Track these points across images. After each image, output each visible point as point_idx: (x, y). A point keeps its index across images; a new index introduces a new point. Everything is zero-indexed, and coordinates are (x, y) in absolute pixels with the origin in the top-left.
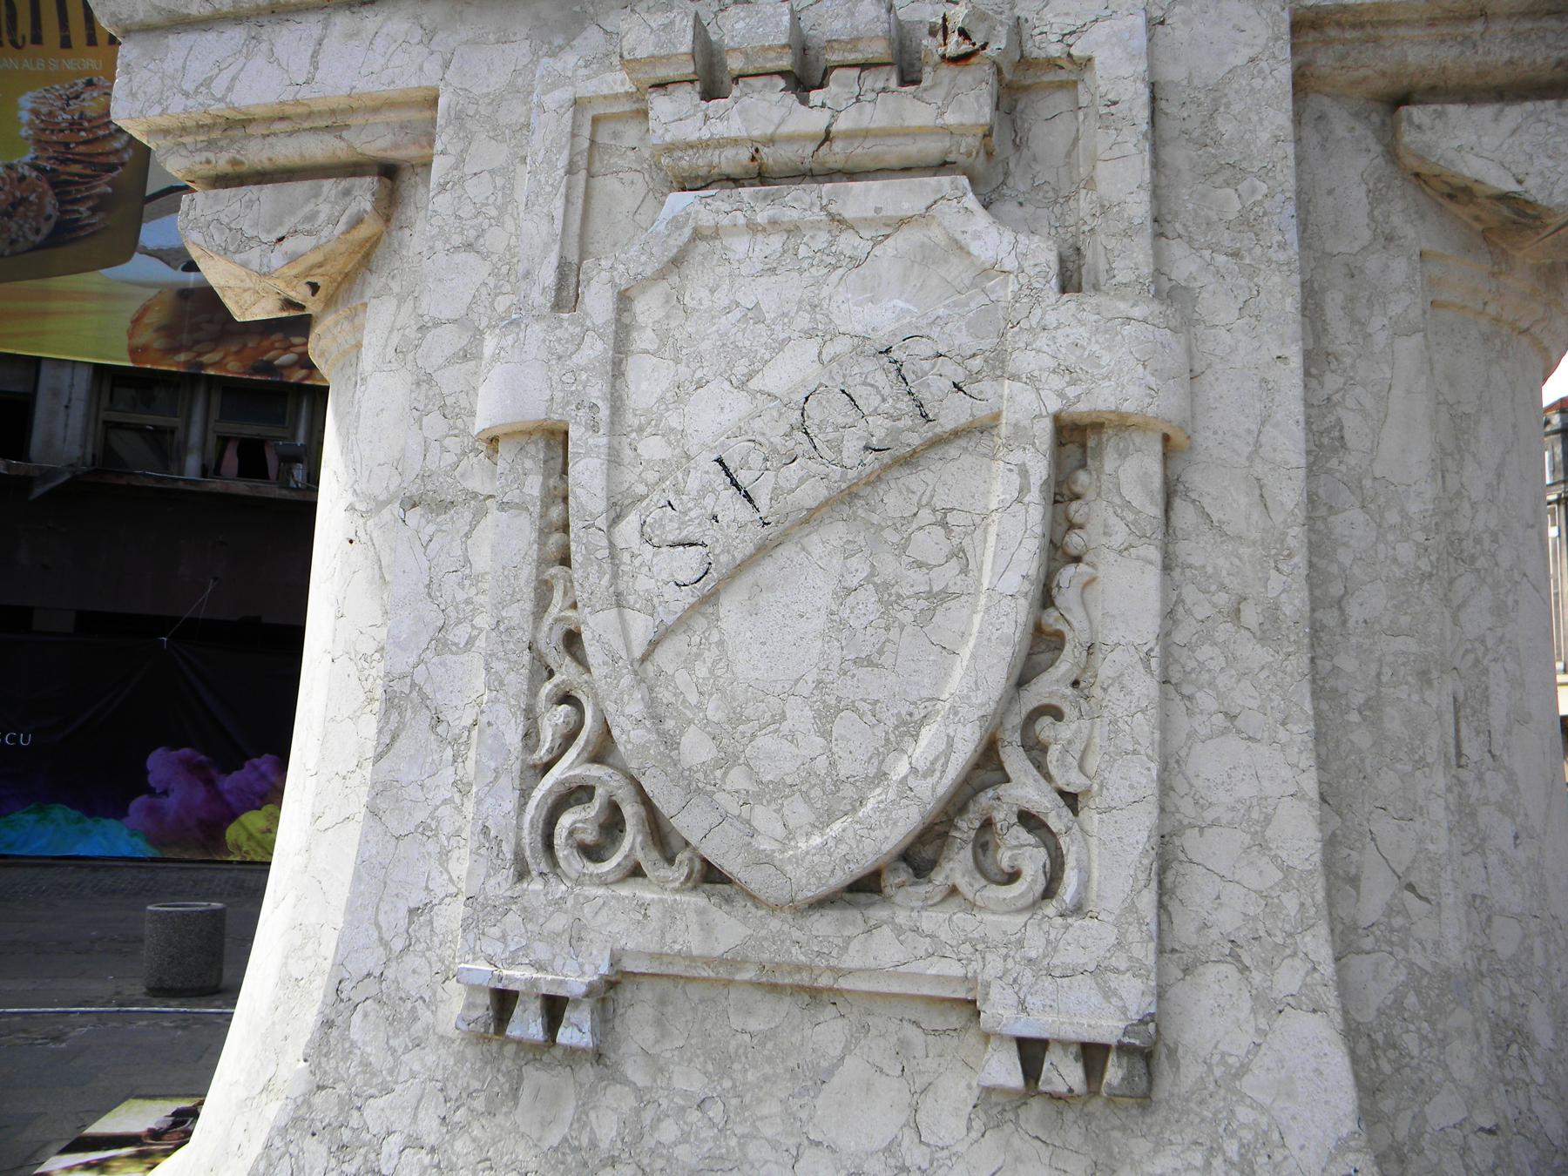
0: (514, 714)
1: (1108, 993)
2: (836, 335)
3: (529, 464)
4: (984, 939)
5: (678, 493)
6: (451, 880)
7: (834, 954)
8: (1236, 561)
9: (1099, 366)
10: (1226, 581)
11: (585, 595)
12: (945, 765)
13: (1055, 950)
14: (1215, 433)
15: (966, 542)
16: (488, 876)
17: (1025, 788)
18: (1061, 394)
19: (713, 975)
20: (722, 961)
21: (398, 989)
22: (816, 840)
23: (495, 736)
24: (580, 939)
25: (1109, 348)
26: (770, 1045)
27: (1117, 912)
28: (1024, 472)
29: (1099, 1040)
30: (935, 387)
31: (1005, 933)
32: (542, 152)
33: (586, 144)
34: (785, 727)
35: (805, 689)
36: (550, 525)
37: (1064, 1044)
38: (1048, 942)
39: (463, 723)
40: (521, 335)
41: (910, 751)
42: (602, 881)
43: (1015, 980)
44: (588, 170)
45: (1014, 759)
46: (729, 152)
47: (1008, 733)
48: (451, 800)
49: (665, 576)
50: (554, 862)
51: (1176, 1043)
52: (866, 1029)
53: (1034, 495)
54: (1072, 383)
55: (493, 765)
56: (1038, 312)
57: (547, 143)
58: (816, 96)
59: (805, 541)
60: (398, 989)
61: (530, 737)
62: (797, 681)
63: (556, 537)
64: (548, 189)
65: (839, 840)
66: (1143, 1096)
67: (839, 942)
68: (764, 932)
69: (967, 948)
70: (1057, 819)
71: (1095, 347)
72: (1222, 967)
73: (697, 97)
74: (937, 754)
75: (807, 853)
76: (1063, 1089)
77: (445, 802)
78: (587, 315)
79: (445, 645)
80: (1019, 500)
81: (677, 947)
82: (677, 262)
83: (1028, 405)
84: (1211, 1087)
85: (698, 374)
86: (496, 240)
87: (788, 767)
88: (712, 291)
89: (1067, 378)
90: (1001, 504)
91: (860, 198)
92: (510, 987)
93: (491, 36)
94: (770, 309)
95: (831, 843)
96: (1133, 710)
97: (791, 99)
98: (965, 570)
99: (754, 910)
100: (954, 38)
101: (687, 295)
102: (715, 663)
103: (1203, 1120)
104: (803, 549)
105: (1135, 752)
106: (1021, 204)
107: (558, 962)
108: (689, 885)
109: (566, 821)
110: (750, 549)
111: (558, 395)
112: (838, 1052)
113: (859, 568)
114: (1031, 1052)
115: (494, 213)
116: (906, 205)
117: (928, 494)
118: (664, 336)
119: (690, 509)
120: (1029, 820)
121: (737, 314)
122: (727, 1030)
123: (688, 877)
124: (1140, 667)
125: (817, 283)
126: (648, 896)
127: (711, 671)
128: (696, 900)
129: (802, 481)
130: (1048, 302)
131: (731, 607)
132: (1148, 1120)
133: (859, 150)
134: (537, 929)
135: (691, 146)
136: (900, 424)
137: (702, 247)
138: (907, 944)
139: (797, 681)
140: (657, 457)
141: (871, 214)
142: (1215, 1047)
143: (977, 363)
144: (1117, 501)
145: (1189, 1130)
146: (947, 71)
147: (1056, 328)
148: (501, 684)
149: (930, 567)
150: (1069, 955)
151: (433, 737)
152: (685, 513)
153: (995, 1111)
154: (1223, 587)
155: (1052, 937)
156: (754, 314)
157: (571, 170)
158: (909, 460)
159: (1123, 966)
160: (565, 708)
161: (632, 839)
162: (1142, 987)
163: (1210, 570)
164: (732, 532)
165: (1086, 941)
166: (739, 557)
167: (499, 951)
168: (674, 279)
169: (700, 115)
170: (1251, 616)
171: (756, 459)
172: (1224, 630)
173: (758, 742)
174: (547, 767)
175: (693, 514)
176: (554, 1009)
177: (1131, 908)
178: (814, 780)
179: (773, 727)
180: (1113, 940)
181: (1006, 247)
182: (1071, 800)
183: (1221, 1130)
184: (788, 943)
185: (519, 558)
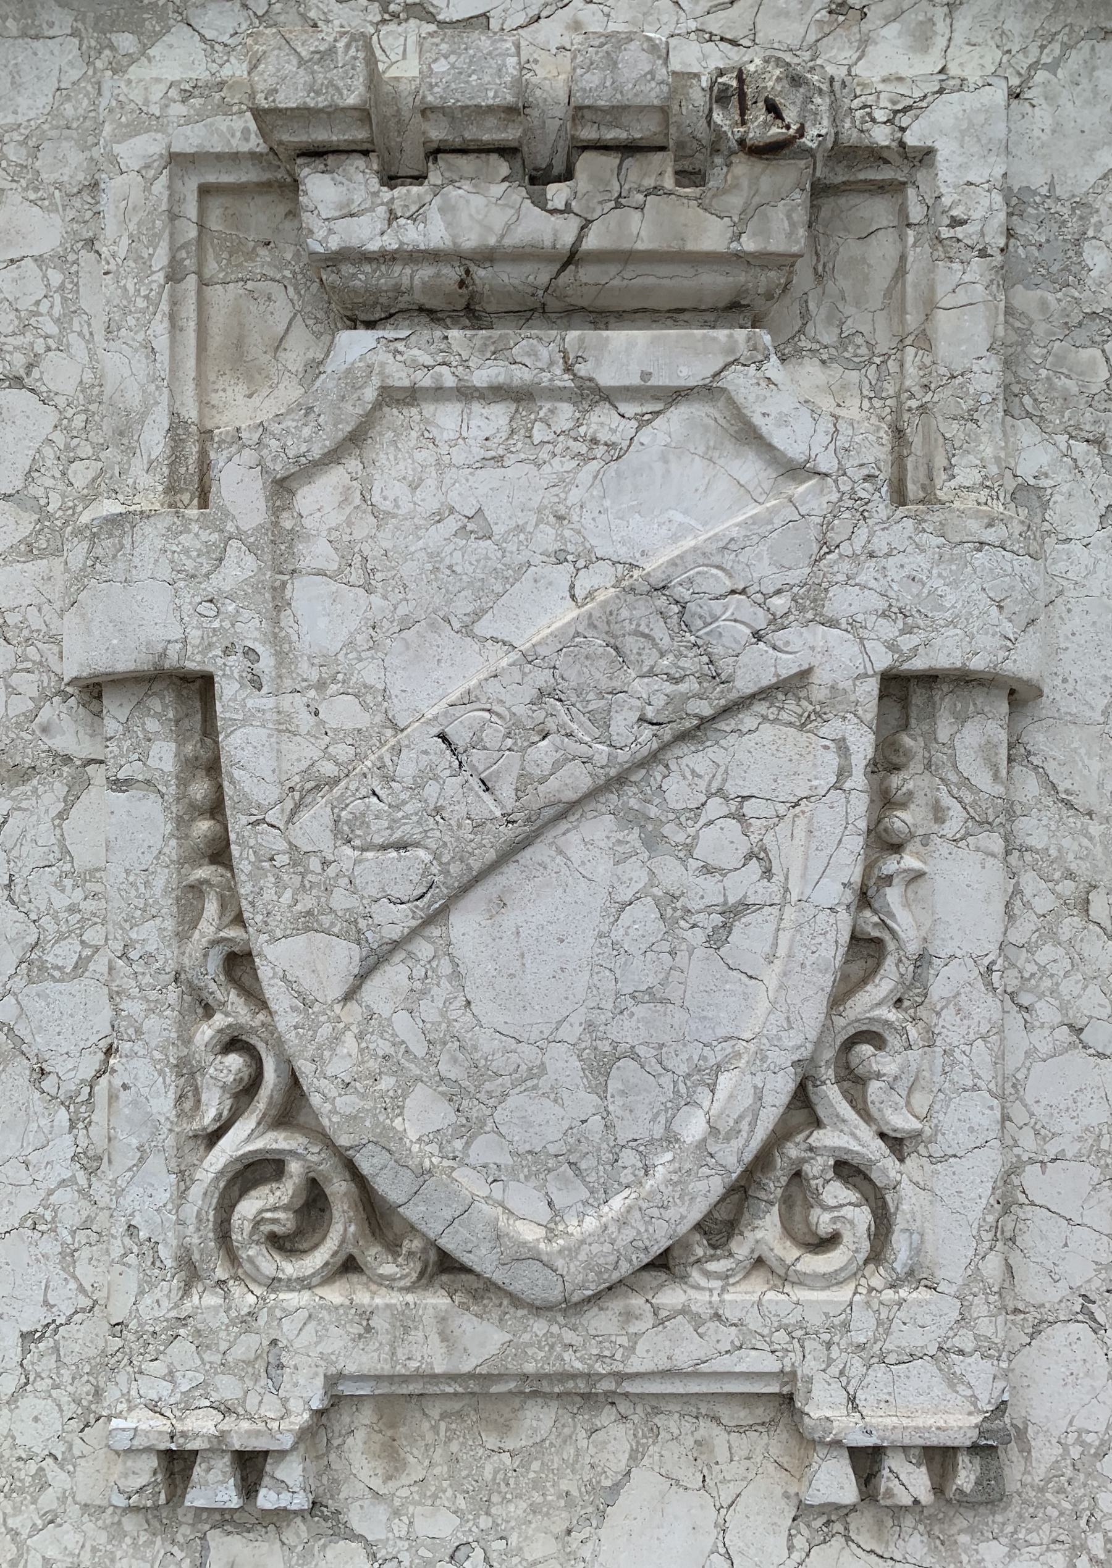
0: (161, 1073)
1: (953, 1380)
2: (592, 559)
3: (152, 725)
4: (801, 1324)
5: (388, 779)
6: (81, 1289)
7: (618, 1356)
8: (1085, 842)
9: (941, 608)
10: (1073, 867)
11: (259, 918)
12: (753, 1124)
13: (888, 1332)
14: (1065, 681)
15: (768, 839)
16: (142, 1293)
17: (844, 1133)
18: (892, 646)
19: (460, 1390)
20: (471, 1376)
21: (14, 1446)
22: (591, 1223)
23: (135, 1103)
24: (280, 1366)
25: (954, 584)
26: (536, 1465)
27: (960, 1282)
28: (842, 747)
29: (949, 1444)
31: (826, 1314)
32: (125, 241)
33: (193, 233)
34: (544, 1083)
35: (571, 1032)
36: (192, 806)
38: (879, 1322)
39: (80, 1076)
40: (127, 541)
41: (706, 1104)
43: (842, 1373)
44: (199, 274)
45: (831, 1096)
46: (425, 272)
47: (823, 1070)
48: (73, 1180)
49: (374, 893)
50: (233, 1258)
51: (1026, 1422)
52: (656, 1431)
53: (858, 780)
54: (908, 630)
55: (135, 1142)
56: (863, 533)
57: (132, 226)
59: (560, 841)
60: (14, 1446)
61: (188, 1097)
62: (560, 1023)
63: (204, 826)
64: (141, 303)
65: (622, 1222)
66: (991, 1496)
67: (624, 1340)
68: (526, 1337)
69: (781, 1337)
70: (886, 1167)
71: (938, 583)
72: (1073, 1327)
73: (374, 182)
74: (744, 1100)
75: (583, 1242)
76: (907, 1501)
77: (63, 1183)
78: (227, 514)
79: (42, 968)
80: (836, 787)
81: (413, 1365)
82: (356, 439)
83: (846, 663)
84: (1069, 1472)
85: (402, 610)
86: (61, 374)
87: (553, 1133)
88: (414, 487)
89: (900, 624)
90: (798, 778)
91: (624, 353)
92: (189, 1446)
93: (10, 23)
94: (501, 521)
95: (613, 1228)
96: (972, 1037)
98: (768, 873)
99: (512, 1310)
101: (376, 491)
102: (448, 1002)
103: (1061, 1514)
104: (560, 852)
105: (975, 1088)
106: (823, 362)
107: (252, 1401)
108: (424, 1281)
109: (248, 1207)
110: (491, 855)
111: (194, 635)
112: (623, 1466)
113: (636, 875)
114: (867, 1461)
115: (52, 329)
116: (684, 371)
117: (719, 777)
118: (347, 553)
119: (404, 802)
120: (848, 1170)
121: (452, 524)
122: (481, 1451)
123: (422, 1274)
124: (980, 984)
125: (562, 482)
126: (363, 1297)
127: (443, 1014)
128: (436, 1300)
129: (557, 766)
130: (876, 518)
131: (466, 925)
132: (999, 1518)
133: (616, 282)
134: (218, 1359)
135: (367, 258)
136: (683, 687)
137: (393, 415)
138: (730, 1319)
139: (560, 1023)
140: (349, 726)
141: (636, 381)
142: (1071, 1423)
143: (780, 603)
144: (953, 777)
145: (1046, 1527)
146: (742, 167)
147: (888, 555)
148: (139, 1031)
149: (724, 872)
150: (905, 1337)
151: (37, 1094)
152: (398, 807)
153: (818, 1523)
154: (1070, 875)
155: (883, 1316)
156: (476, 527)
157: (174, 276)
158: (697, 731)
159: (969, 1347)
160: (235, 1061)
161: (342, 1229)
162: (994, 1370)
163: (1053, 852)
164: (466, 832)
165: (924, 1317)
166: (476, 866)
167: (165, 1393)
168: (353, 464)
169: (381, 211)
171: (493, 736)
172: (1070, 925)
173: (511, 1102)
174: (213, 1137)
175: (409, 808)
176: (250, 1466)
177: (975, 1276)
178: (584, 1148)
179: (529, 1083)
180: (955, 1315)
181: (823, 439)
182: (896, 1144)
183: (1083, 1523)
184: (558, 1348)
185: (149, 857)
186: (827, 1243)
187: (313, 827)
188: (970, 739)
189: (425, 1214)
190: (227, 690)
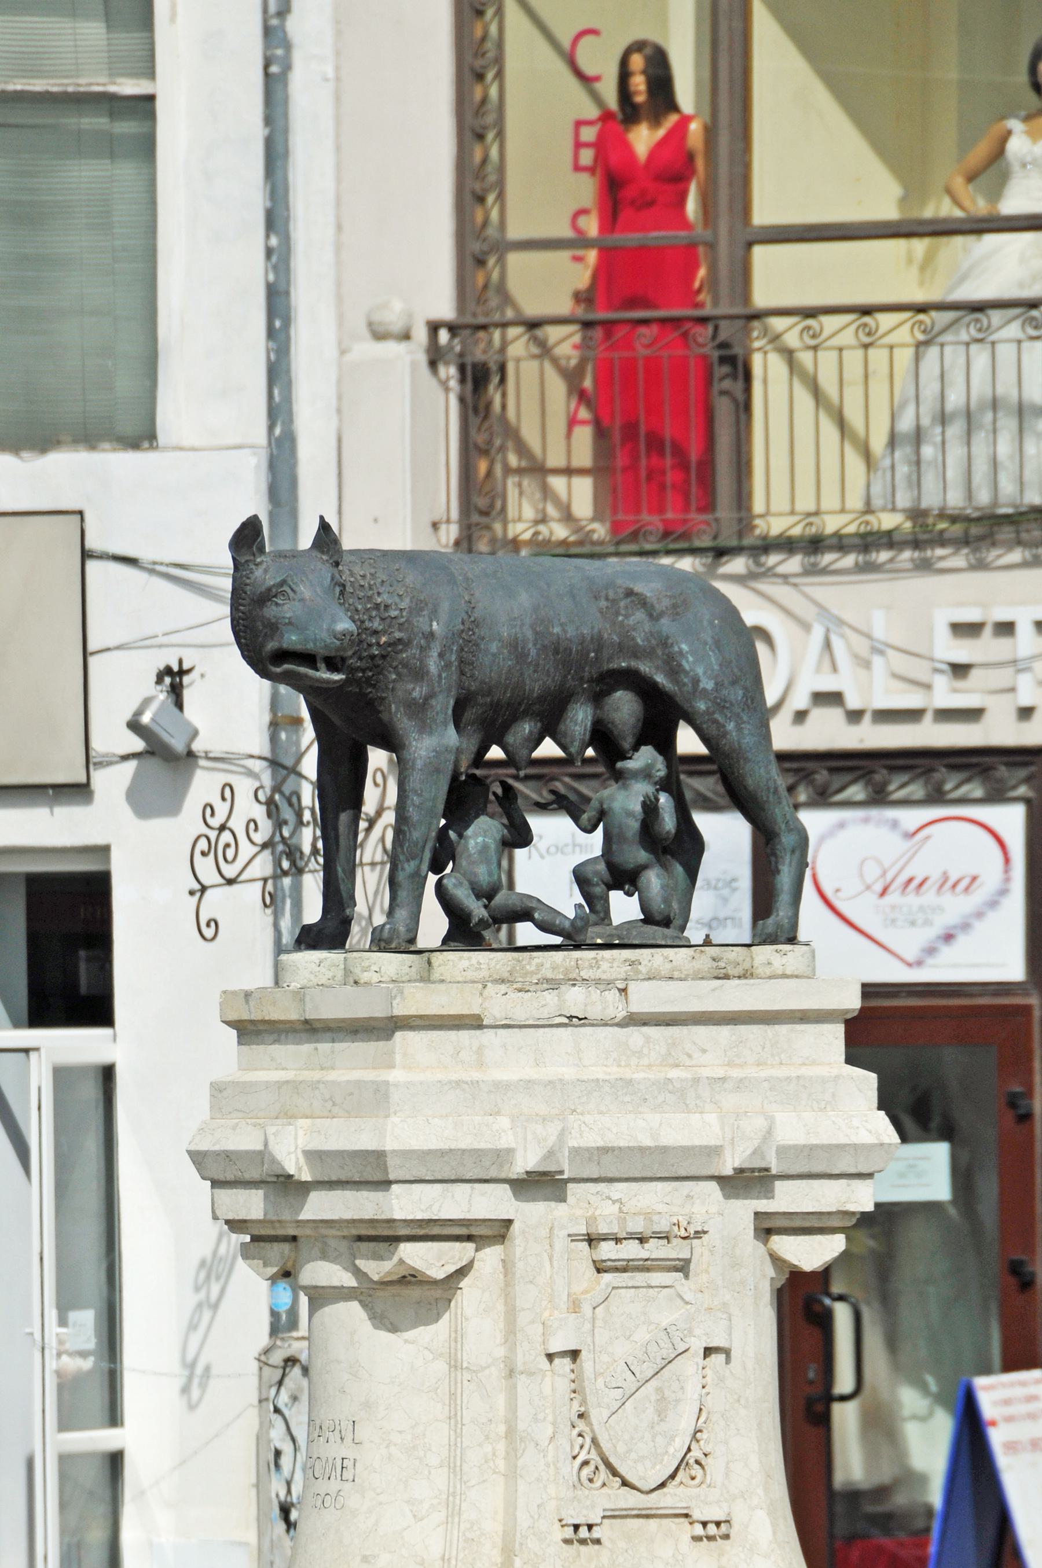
30: (677, 1341)
37: (712, 1522)
42: (597, 1489)
58: (646, 1245)
61: (572, 1446)
83: (698, 1346)
97: (640, 1246)
100: (682, 1230)
114: (704, 1524)
120: (697, 1462)
138: (671, 1498)
170: (743, 1401)
176: (590, 1527)
186: (693, 1478)
187: (600, 1381)
188: (718, 1359)
189: (622, 1470)
190: (584, 1355)
